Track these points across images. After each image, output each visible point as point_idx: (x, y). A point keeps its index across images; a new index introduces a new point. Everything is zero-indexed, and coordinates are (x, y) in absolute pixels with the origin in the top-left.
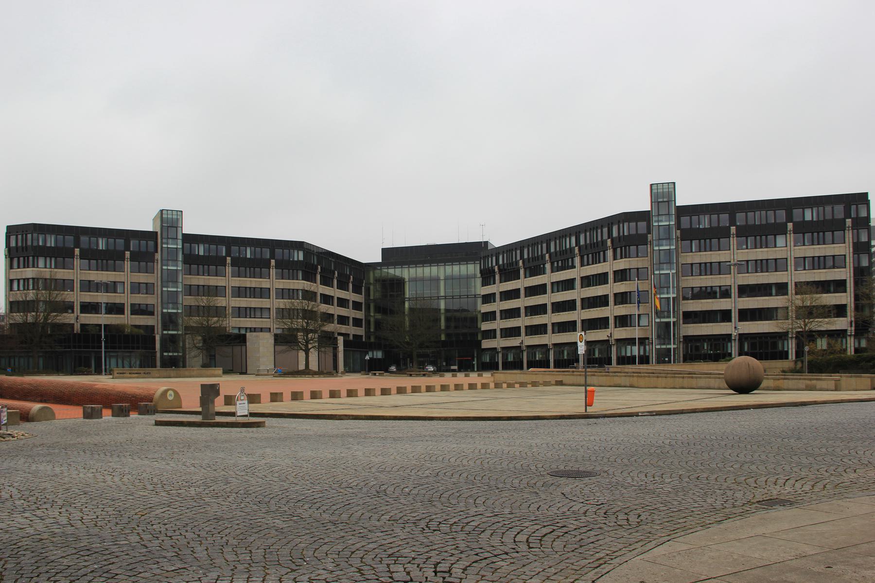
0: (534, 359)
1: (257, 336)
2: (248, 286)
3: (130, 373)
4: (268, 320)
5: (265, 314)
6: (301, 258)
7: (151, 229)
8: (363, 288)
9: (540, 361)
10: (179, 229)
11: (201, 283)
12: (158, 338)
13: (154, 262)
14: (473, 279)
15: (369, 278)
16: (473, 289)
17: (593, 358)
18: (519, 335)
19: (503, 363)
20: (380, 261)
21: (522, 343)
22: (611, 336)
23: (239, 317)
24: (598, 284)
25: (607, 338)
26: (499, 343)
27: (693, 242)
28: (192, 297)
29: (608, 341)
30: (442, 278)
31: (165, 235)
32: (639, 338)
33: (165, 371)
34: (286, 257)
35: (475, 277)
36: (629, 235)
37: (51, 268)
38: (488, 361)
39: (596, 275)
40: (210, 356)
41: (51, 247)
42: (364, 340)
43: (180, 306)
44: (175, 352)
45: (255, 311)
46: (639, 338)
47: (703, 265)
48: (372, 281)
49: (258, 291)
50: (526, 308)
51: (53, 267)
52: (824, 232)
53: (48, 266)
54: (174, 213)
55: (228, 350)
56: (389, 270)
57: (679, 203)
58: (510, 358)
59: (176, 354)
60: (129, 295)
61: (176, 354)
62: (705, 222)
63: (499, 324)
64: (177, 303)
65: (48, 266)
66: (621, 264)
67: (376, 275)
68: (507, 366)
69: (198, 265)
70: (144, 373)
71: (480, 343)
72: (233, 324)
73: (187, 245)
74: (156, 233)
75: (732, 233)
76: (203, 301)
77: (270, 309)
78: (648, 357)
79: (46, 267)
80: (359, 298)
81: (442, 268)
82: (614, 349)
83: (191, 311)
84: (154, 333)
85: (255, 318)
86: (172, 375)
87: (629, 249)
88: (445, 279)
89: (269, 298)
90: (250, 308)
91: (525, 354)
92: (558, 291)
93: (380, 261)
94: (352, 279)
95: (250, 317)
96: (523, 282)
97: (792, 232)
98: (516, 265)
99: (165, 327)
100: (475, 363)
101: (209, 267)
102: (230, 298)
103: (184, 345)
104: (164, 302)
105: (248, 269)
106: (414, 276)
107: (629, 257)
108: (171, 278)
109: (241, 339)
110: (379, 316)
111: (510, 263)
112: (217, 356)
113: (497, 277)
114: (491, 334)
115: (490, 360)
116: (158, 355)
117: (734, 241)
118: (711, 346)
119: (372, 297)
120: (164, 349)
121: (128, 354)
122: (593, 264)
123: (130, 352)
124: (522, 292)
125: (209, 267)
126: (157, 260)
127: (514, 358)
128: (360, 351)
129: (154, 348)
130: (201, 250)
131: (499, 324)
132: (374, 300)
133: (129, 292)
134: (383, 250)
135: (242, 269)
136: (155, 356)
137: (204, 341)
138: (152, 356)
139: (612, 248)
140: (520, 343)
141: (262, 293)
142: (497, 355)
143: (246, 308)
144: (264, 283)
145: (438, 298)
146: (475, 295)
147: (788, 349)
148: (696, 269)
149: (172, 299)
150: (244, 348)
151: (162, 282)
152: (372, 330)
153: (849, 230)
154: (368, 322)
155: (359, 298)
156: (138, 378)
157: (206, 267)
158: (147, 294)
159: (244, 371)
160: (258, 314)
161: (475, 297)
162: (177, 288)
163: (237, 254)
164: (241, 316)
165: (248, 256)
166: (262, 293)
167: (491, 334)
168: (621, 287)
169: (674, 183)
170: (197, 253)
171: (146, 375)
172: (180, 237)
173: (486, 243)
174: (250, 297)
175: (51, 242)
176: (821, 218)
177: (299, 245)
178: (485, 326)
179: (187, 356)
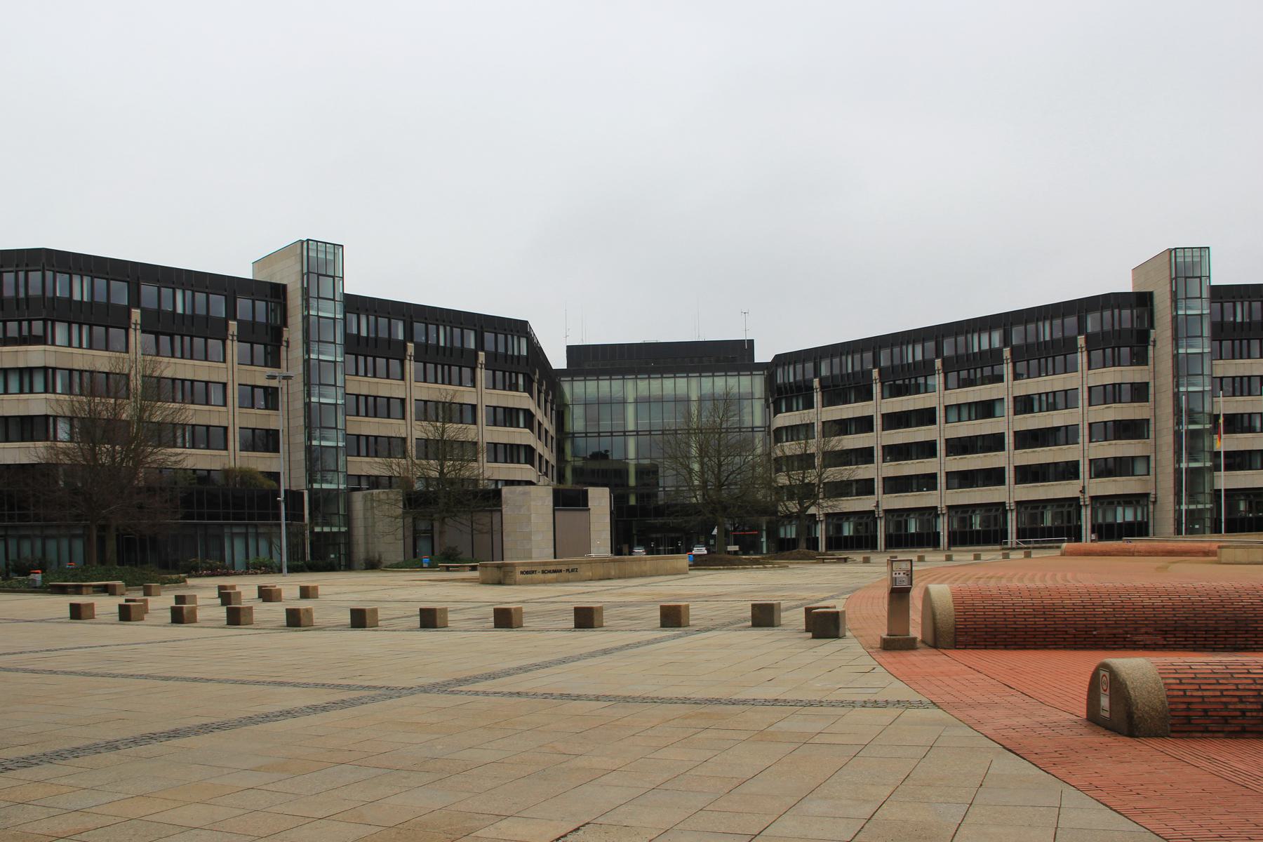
0: (903, 532)
1: (525, 493)
3: (543, 572)
10: (339, 283)
17: (1044, 528)
20: (756, 361)
21: (1083, 491)
22: (1084, 493)
30: (631, 399)
32: (1225, 490)
35: (751, 397)
37: (81, 346)
41: (82, 302)
45: (792, 430)
46: (1225, 490)
47: (1238, 380)
51: (85, 345)
52: (1249, 340)
53: (75, 342)
57: (1216, 281)
58: (848, 530)
59: (326, 529)
60: (237, 409)
62: (1046, 332)
65: (75, 342)
66: (1110, 375)
70: (568, 570)
72: (491, 471)
75: (1079, 346)
78: (1147, 524)
79: (70, 345)
81: (694, 382)
87: (1119, 351)
92: (970, 419)
93: (756, 361)
96: (879, 406)
106: (646, 393)
109: (491, 498)
117: (938, 380)
121: (243, 530)
123: (271, 525)
127: (856, 530)
133: (237, 404)
134: (568, 346)
139: (1012, 361)
144: (466, 395)
145: (625, 433)
147: (1148, 519)
148: (1228, 386)
150: (496, 516)
153: (1082, 352)
156: (557, 581)
163: (423, 338)
165: (180, 310)
169: (1208, 248)
171: (571, 576)
172: (1205, 294)
175: (80, 290)
176: (1247, 320)
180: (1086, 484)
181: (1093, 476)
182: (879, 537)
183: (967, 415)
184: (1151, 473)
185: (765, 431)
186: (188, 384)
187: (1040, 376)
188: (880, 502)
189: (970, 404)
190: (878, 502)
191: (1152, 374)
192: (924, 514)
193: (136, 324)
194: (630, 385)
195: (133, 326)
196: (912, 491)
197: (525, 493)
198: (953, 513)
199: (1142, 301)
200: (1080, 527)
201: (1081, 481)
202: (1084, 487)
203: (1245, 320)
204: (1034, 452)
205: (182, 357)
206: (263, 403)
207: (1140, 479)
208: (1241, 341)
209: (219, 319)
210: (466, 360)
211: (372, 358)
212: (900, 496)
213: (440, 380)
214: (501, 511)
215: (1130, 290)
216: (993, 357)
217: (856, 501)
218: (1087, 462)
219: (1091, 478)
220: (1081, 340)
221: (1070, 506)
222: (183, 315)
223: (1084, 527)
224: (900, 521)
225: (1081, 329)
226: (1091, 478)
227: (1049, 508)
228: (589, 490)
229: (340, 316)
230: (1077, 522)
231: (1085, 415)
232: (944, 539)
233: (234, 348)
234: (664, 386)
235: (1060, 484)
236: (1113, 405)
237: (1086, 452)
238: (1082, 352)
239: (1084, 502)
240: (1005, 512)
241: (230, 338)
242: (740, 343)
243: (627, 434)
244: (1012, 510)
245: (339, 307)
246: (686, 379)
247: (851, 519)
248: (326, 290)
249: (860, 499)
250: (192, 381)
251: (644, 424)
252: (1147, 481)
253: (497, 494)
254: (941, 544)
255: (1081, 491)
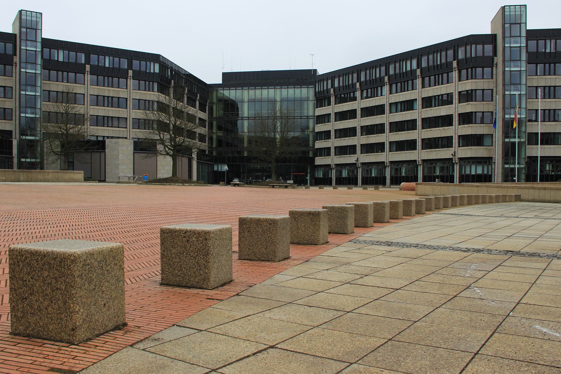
2: (106, 94)
4: (125, 129)
5: (122, 124)
6: (157, 70)
7: (11, 32)
8: (207, 107)
9: (376, 178)
11: (60, 89)
12: (15, 143)
13: (12, 65)
14: (306, 102)
15: (212, 99)
16: (306, 111)
18: (355, 153)
19: (336, 179)
21: (357, 160)
22: (455, 155)
23: (97, 126)
24: (440, 104)
25: (451, 157)
26: (333, 160)
27: (539, 65)
28: (50, 103)
29: (355, 164)
30: (246, 100)
31: (23, 37)
33: (23, 174)
34: (143, 69)
35: (307, 99)
36: (476, 56)
38: (321, 176)
39: (404, 102)
40: (69, 162)
42: (207, 153)
43: (38, 111)
44: (33, 158)
47: (547, 89)
48: (215, 101)
49: (101, 119)
50: (362, 127)
54: (34, 14)
55: (87, 156)
56: (225, 91)
58: (345, 174)
59: (33, 160)
61: (33, 160)
62: (440, 59)
63: (333, 143)
64: (35, 108)
66: (468, 85)
67: (219, 95)
68: (341, 182)
69: (57, 71)
71: (313, 160)
73: (46, 50)
74: (15, 35)
76: (61, 108)
77: (126, 118)
80: (204, 116)
81: (278, 91)
82: (457, 168)
83: (48, 116)
84: (12, 138)
85: (112, 127)
86: (22, 178)
88: (281, 101)
89: (126, 108)
90: (108, 117)
91: (360, 171)
94: (198, 98)
95: (108, 126)
97: (131, 78)
98: (327, 93)
99: (23, 133)
100: (308, 178)
101: (68, 74)
102: (89, 107)
103: (42, 150)
104: (21, 106)
105: (106, 78)
106: (253, 97)
107: (475, 79)
108: (30, 81)
110: (220, 134)
111: (346, 86)
112: (75, 162)
113: (333, 99)
114: (326, 152)
115: (323, 175)
116: (15, 160)
117: (386, 89)
118: (553, 167)
119: (214, 115)
120: (21, 154)
122: (401, 92)
124: (359, 113)
125: (68, 74)
126: (16, 63)
127: (348, 174)
128: (208, 164)
129: (11, 153)
130: (61, 56)
131: (333, 143)
132: (218, 119)
135: (101, 78)
136: (12, 162)
137: (63, 146)
138: (8, 162)
140: (356, 161)
141: (120, 103)
142: (330, 171)
143: (104, 117)
144: (122, 93)
146: (308, 116)
147: (492, 173)
149: (31, 103)
150: (103, 154)
151: (20, 86)
152: (214, 146)
153: (455, 71)
154: (211, 139)
155: (204, 116)
157: (65, 73)
158: (5, 97)
159: (103, 179)
160: (116, 123)
161: (308, 118)
162: (36, 92)
163: (96, 63)
164: (99, 124)
165: (107, 65)
166: (120, 103)
167: (326, 152)
168: (467, 107)
169: (526, 5)
170: (56, 59)
172: (524, 34)
173: (315, 71)
174: (108, 106)
177: (156, 58)
178: (319, 144)
179: (45, 162)
180: (456, 151)
181: (461, 146)
182: (359, 178)
183: (395, 110)
184: (13, 120)
185: (314, 118)
186: (110, 98)
187: (435, 85)
188: (456, 152)
189: (401, 102)
190: (358, 158)
191: (495, 84)
192: (410, 165)
193: (88, 72)
194: (246, 92)
195: (129, 78)
196: (374, 153)
197: (116, 143)
198: (425, 164)
199: (491, 39)
200: (454, 176)
201: (454, 148)
202: (455, 152)
203: (552, 51)
204: (431, 130)
205: (108, 86)
206: (3, 95)
207: (486, 149)
208: (550, 64)
209: (125, 69)
210: (121, 74)
211: (111, 78)
212: (368, 155)
213: (106, 84)
214: (105, 152)
215: (490, 33)
216: (411, 75)
217: (349, 157)
218: (457, 137)
219: (459, 146)
220: (455, 64)
221: (448, 163)
222: (109, 68)
223: (455, 176)
224: (397, 168)
225: (455, 57)
226: (459, 146)
227: (438, 164)
228: (13, 141)
229: (39, 49)
230: (452, 173)
231: (456, 109)
232: (388, 181)
233: (131, 82)
234: (262, 93)
235: (444, 150)
236: (471, 103)
237: (456, 131)
238: (455, 71)
239: (455, 161)
240: (453, 165)
241: (14, 64)
242: (310, 71)
243: (243, 118)
244: (457, 163)
245: (39, 45)
246: (274, 90)
247: (347, 168)
248: (31, 37)
249: (350, 156)
250: (112, 97)
251: (252, 113)
252: (491, 149)
253: (103, 142)
254: (387, 183)
255: (452, 154)
